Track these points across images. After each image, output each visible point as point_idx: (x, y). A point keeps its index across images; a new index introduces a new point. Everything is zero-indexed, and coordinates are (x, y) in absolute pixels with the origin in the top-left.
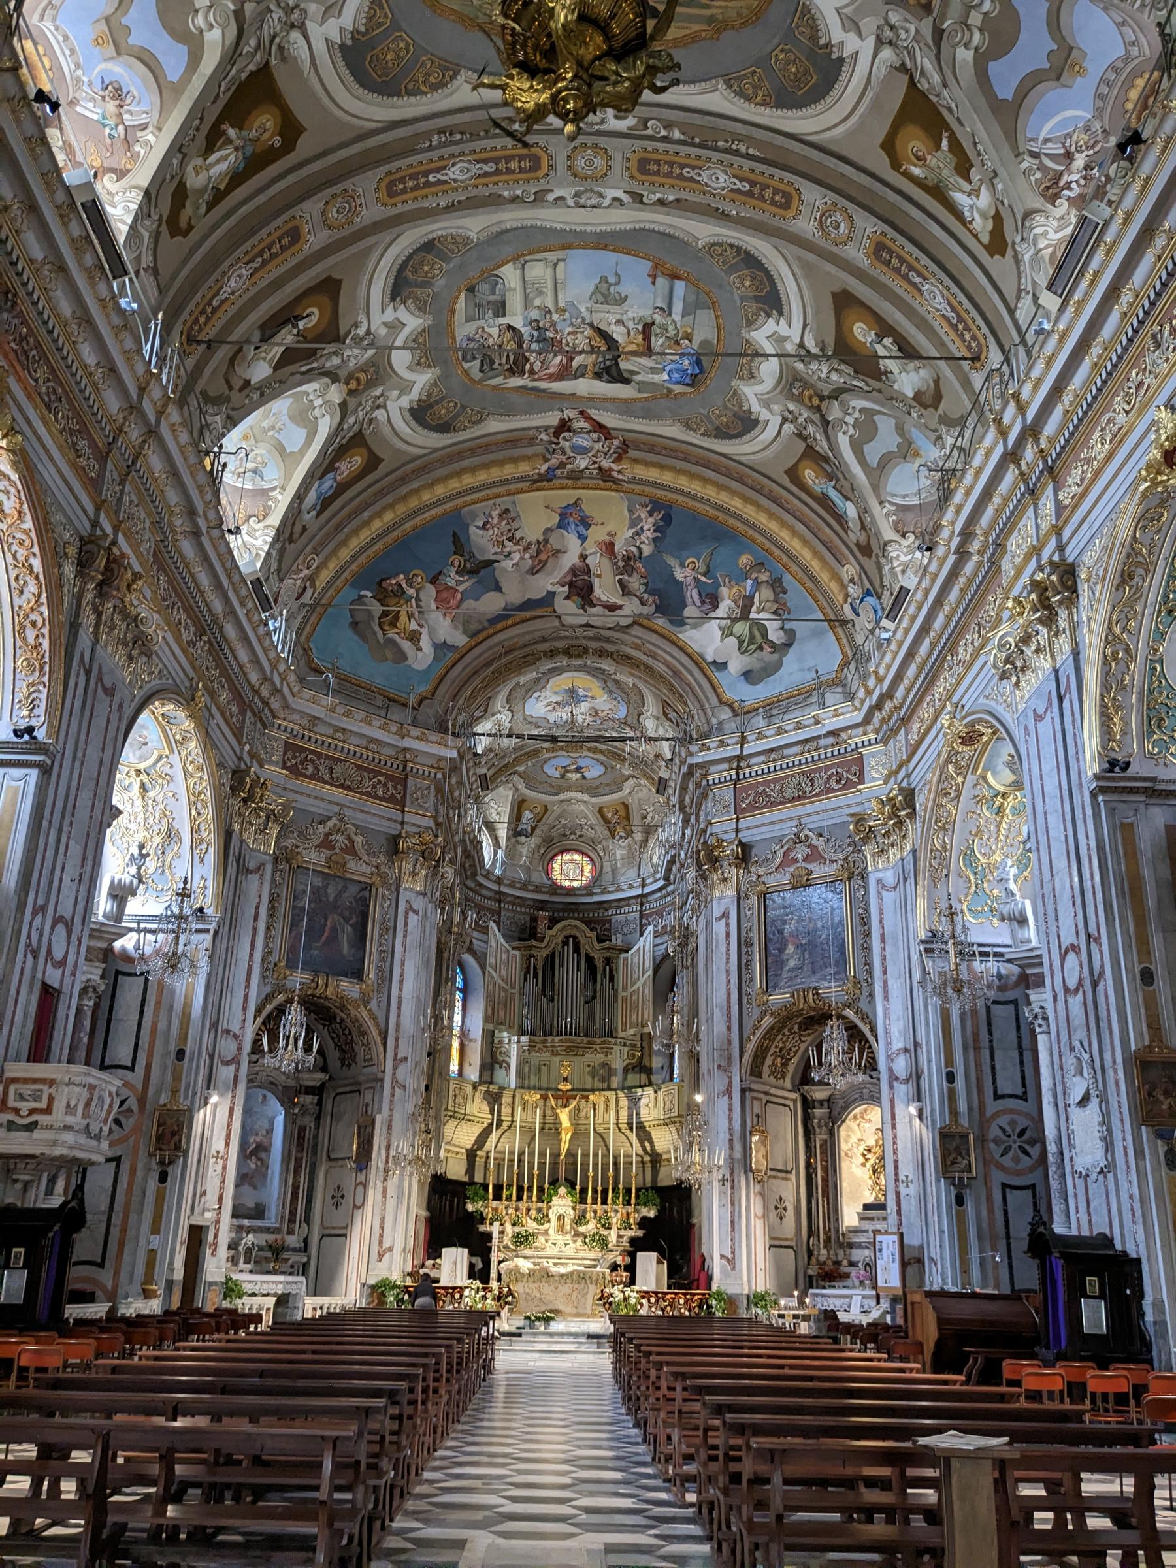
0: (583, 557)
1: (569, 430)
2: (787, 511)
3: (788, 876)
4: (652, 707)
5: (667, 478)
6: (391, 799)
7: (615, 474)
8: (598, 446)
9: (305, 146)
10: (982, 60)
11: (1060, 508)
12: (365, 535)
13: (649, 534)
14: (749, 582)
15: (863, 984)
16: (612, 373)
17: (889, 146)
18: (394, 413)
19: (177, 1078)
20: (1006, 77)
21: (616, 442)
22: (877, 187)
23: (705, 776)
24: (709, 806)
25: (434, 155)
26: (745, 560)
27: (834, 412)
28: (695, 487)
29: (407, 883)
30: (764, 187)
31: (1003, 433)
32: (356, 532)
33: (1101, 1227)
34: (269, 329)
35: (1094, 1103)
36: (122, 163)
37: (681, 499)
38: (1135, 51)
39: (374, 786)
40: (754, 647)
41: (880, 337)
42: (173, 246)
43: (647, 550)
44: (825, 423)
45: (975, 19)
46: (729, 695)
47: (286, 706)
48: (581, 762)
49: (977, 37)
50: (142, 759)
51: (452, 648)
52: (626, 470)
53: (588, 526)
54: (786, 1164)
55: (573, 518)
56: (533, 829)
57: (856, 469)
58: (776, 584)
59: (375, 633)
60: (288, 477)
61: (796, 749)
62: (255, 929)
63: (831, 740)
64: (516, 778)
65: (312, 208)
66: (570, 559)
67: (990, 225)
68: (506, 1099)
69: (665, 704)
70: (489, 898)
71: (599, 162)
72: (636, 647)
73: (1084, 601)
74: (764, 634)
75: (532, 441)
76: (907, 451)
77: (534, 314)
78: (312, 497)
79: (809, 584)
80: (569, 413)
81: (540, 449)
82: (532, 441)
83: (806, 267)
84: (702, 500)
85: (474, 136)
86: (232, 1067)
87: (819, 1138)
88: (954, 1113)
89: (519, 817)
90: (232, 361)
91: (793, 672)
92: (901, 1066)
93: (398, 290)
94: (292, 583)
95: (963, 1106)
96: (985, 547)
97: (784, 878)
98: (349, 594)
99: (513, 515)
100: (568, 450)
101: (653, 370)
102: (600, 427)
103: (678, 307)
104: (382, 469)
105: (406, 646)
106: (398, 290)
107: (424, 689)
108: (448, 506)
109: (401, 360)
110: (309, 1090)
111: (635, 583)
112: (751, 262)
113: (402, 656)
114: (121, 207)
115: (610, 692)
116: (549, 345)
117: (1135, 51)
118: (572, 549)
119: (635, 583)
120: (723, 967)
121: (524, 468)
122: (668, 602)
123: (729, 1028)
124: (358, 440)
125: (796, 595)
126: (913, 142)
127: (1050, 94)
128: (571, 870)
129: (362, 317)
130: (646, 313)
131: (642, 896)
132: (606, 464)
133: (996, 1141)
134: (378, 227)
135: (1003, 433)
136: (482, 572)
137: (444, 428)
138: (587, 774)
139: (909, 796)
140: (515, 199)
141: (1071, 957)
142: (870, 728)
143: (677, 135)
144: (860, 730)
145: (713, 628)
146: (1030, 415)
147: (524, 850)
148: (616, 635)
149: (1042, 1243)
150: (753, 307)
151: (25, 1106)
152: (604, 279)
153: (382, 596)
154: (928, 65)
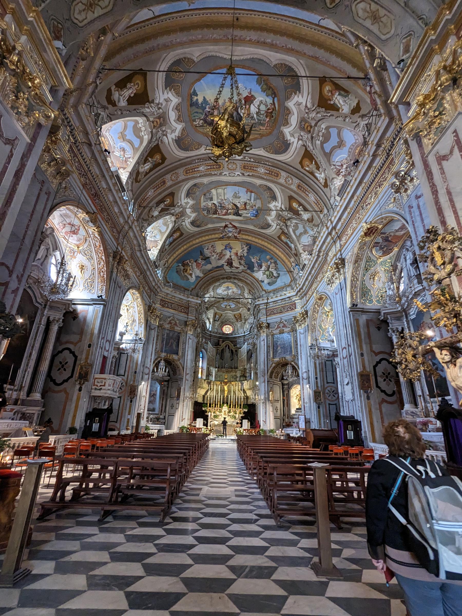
0: (231, 256)
4: (246, 291)
5: (250, 238)
6: (185, 313)
9: (166, 163)
10: (322, 143)
11: (341, 245)
12: (180, 251)
15: (296, 357)
16: (237, 214)
17: (301, 163)
18: (187, 223)
19: (135, 378)
20: (328, 147)
22: (298, 172)
24: (260, 314)
25: (196, 164)
26: (268, 257)
27: (289, 223)
28: (256, 240)
29: (189, 332)
30: (272, 172)
31: (328, 228)
32: (178, 250)
33: (352, 414)
34: (158, 204)
35: (350, 384)
36: (125, 166)
38: (357, 141)
41: (299, 206)
42: (136, 185)
43: (245, 255)
44: (287, 226)
45: (321, 134)
46: (265, 288)
47: (161, 291)
48: (230, 304)
49: (321, 138)
50: (127, 303)
51: (200, 277)
52: (240, 236)
53: (232, 249)
55: (228, 247)
57: (294, 236)
58: (275, 263)
60: (162, 238)
65: (168, 176)
66: (227, 257)
67: (324, 181)
68: (212, 383)
69: (250, 290)
71: (234, 166)
73: (346, 267)
74: (273, 274)
75: (219, 229)
76: (305, 232)
77: (219, 201)
78: (167, 242)
80: (227, 223)
81: (220, 231)
82: (219, 229)
83: (282, 190)
85: (206, 160)
88: (317, 387)
90: (149, 211)
91: (279, 283)
92: (305, 375)
93: (188, 195)
94: (163, 262)
95: (319, 385)
96: (324, 254)
97: (278, 331)
98: (176, 265)
101: (247, 213)
102: (234, 226)
103: (252, 199)
105: (189, 277)
106: (188, 195)
107: (193, 287)
109: (188, 211)
110: (166, 381)
111: (242, 262)
112: (269, 189)
114: (124, 176)
116: (223, 207)
117: (357, 141)
119: (242, 262)
121: (217, 236)
122: (250, 267)
124: (178, 229)
125: (280, 265)
126: (306, 162)
127: (338, 151)
129: (179, 201)
130: (245, 200)
132: (236, 235)
133: (327, 393)
134: (183, 181)
135: (328, 228)
137: (198, 226)
139: (307, 312)
140: (215, 174)
141: (344, 350)
143: (252, 160)
145: (261, 273)
146: (334, 224)
149: (338, 417)
150: (270, 199)
151: (99, 384)
152: (235, 193)
153: (184, 265)
154: (310, 145)
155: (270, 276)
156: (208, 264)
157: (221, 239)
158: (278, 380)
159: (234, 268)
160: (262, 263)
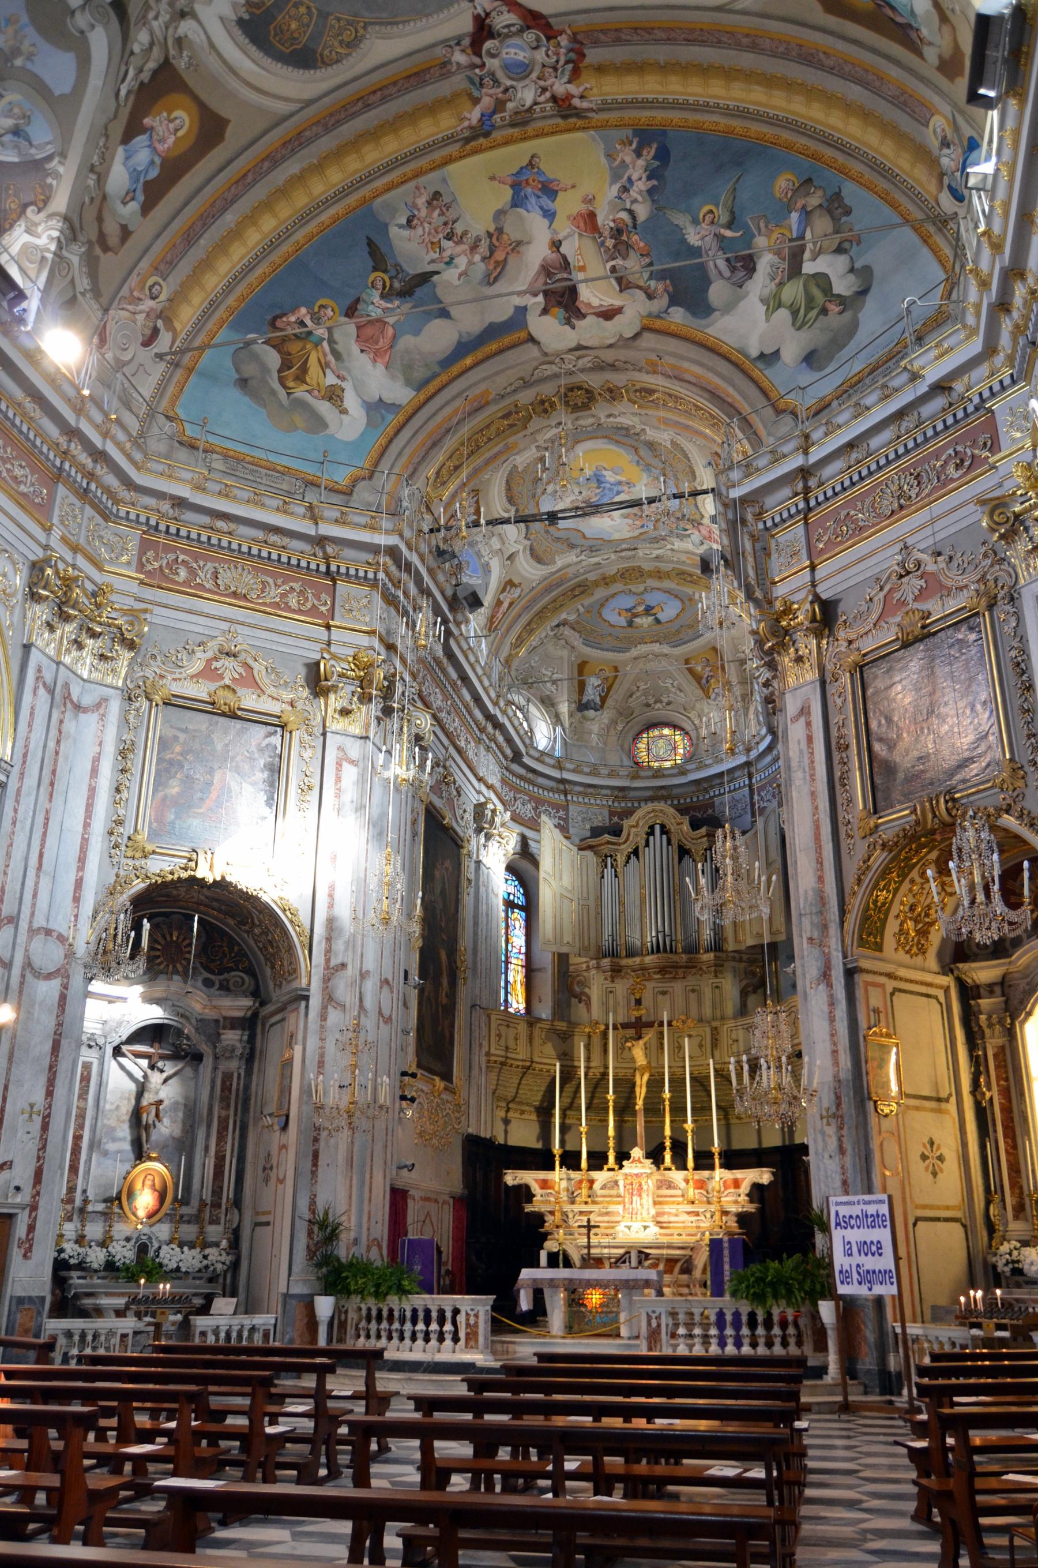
0: (556, 245)
1: (491, 35)
2: (831, 70)
3: (895, 629)
5: (650, 87)
6: (313, 612)
7: (576, 102)
8: (540, 56)
13: (641, 186)
14: (795, 216)
21: (563, 40)
23: (759, 516)
26: (783, 183)
28: (694, 90)
37: (675, 116)
39: (283, 596)
40: (813, 313)
43: (643, 212)
48: (652, 599)
51: (393, 407)
54: (936, 1086)
55: (531, 187)
56: (603, 700)
58: (836, 207)
59: (273, 393)
60: (66, 135)
61: (887, 435)
62: (92, 791)
63: (939, 402)
64: (567, 631)
66: (538, 253)
70: (551, 790)
72: (653, 369)
78: (118, 177)
79: (883, 184)
84: (706, 108)
86: (56, 984)
87: (992, 1043)
89: (582, 687)
99: (446, 199)
100: (500, 75)
104: (233, 138)
108: (352, 200)
110: (234, 1023)
111: (632, 264)
113: (318, 424)
115: (648, 467)
118: (537, 236)
120: (806, 790)
121: (446, 123)
122: (689, 290)
123: (821, 879)
128: (661, 748)
131: (748, 764)
132: (560, 87)
136: (419, 292)
137: (304, 59)
138: (661, 616)
142: (1000, 359)
144: (984, 369)
147: (595, 728)
148: (622, 354)
155: (810, 299)
156: (430, 316)
157: (478, 137)
158: (932, 962)
159: (591, 320)
160: (748, 239)
